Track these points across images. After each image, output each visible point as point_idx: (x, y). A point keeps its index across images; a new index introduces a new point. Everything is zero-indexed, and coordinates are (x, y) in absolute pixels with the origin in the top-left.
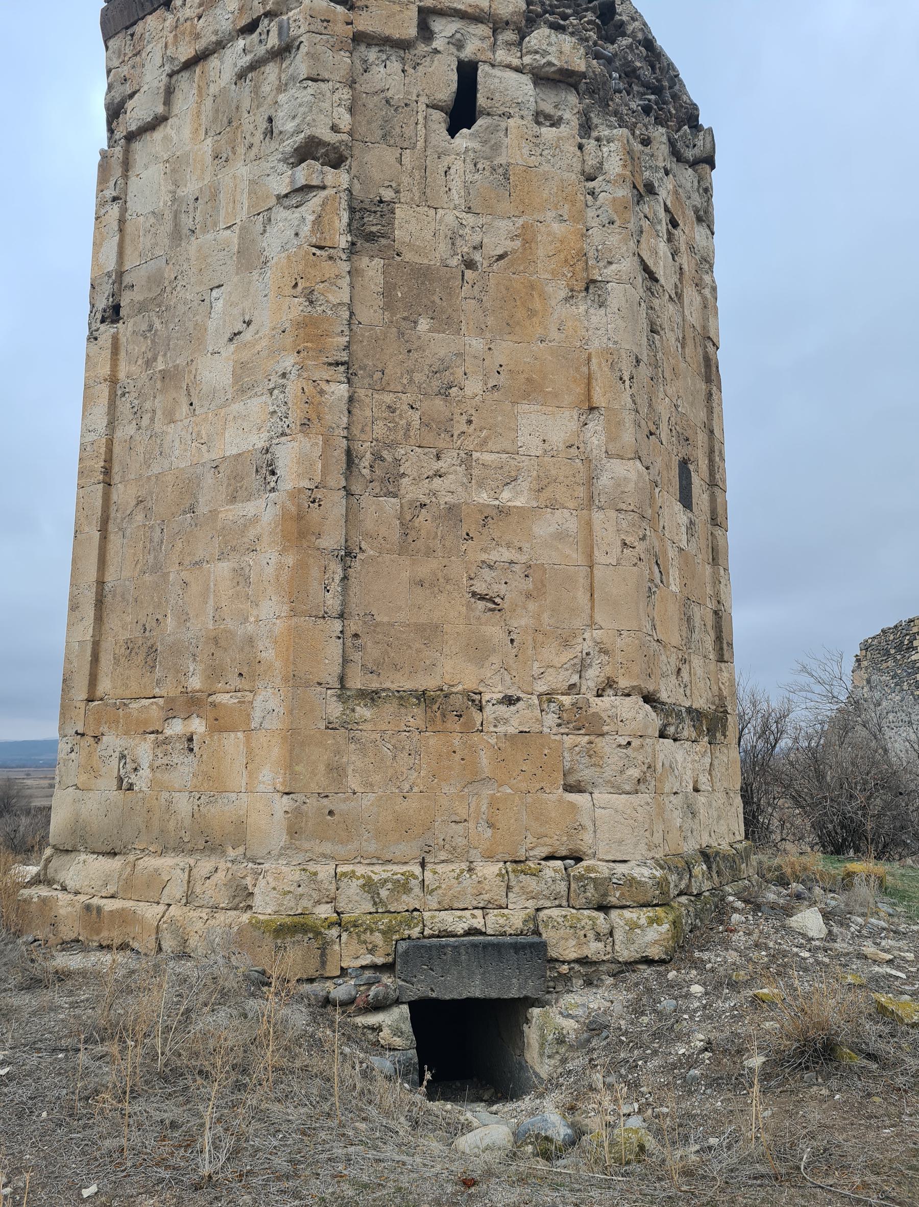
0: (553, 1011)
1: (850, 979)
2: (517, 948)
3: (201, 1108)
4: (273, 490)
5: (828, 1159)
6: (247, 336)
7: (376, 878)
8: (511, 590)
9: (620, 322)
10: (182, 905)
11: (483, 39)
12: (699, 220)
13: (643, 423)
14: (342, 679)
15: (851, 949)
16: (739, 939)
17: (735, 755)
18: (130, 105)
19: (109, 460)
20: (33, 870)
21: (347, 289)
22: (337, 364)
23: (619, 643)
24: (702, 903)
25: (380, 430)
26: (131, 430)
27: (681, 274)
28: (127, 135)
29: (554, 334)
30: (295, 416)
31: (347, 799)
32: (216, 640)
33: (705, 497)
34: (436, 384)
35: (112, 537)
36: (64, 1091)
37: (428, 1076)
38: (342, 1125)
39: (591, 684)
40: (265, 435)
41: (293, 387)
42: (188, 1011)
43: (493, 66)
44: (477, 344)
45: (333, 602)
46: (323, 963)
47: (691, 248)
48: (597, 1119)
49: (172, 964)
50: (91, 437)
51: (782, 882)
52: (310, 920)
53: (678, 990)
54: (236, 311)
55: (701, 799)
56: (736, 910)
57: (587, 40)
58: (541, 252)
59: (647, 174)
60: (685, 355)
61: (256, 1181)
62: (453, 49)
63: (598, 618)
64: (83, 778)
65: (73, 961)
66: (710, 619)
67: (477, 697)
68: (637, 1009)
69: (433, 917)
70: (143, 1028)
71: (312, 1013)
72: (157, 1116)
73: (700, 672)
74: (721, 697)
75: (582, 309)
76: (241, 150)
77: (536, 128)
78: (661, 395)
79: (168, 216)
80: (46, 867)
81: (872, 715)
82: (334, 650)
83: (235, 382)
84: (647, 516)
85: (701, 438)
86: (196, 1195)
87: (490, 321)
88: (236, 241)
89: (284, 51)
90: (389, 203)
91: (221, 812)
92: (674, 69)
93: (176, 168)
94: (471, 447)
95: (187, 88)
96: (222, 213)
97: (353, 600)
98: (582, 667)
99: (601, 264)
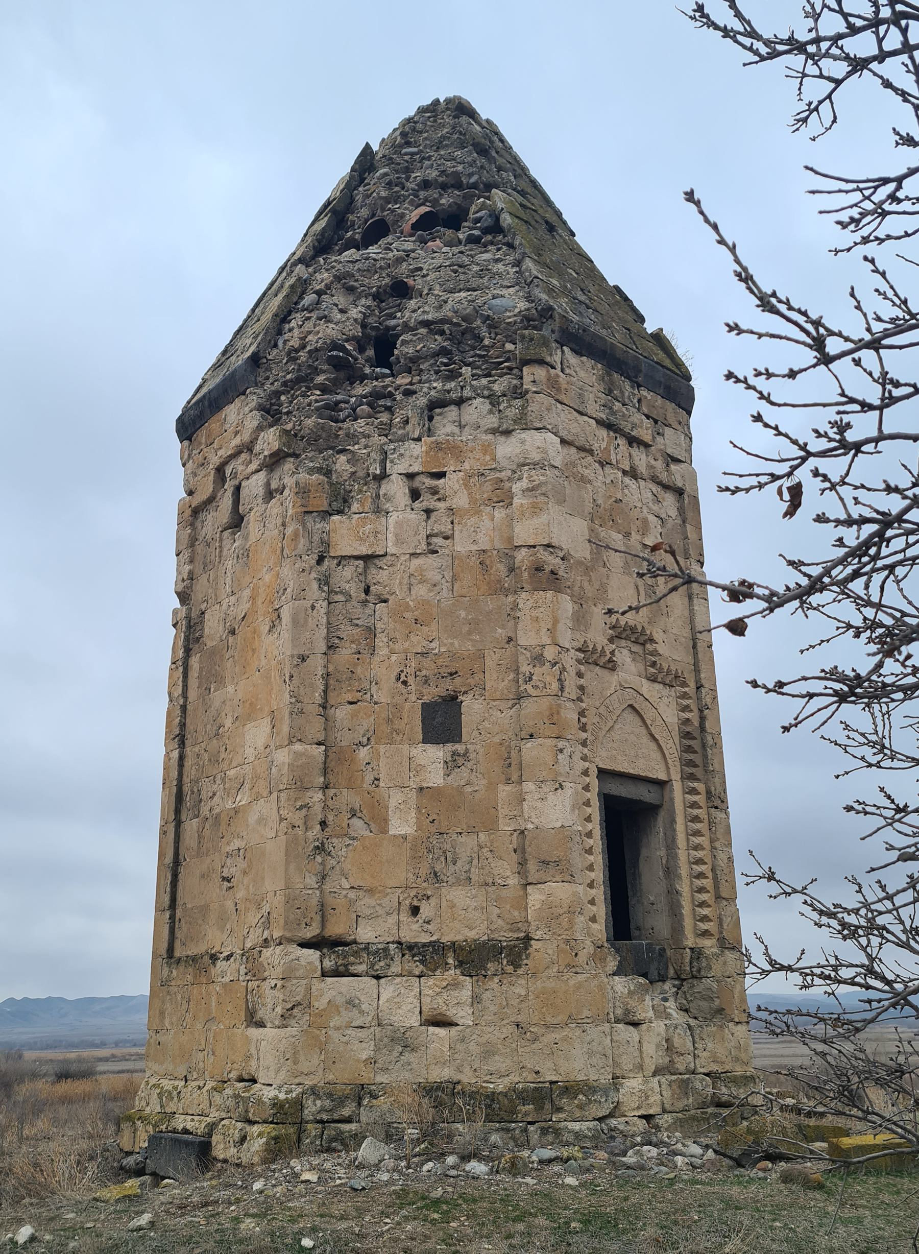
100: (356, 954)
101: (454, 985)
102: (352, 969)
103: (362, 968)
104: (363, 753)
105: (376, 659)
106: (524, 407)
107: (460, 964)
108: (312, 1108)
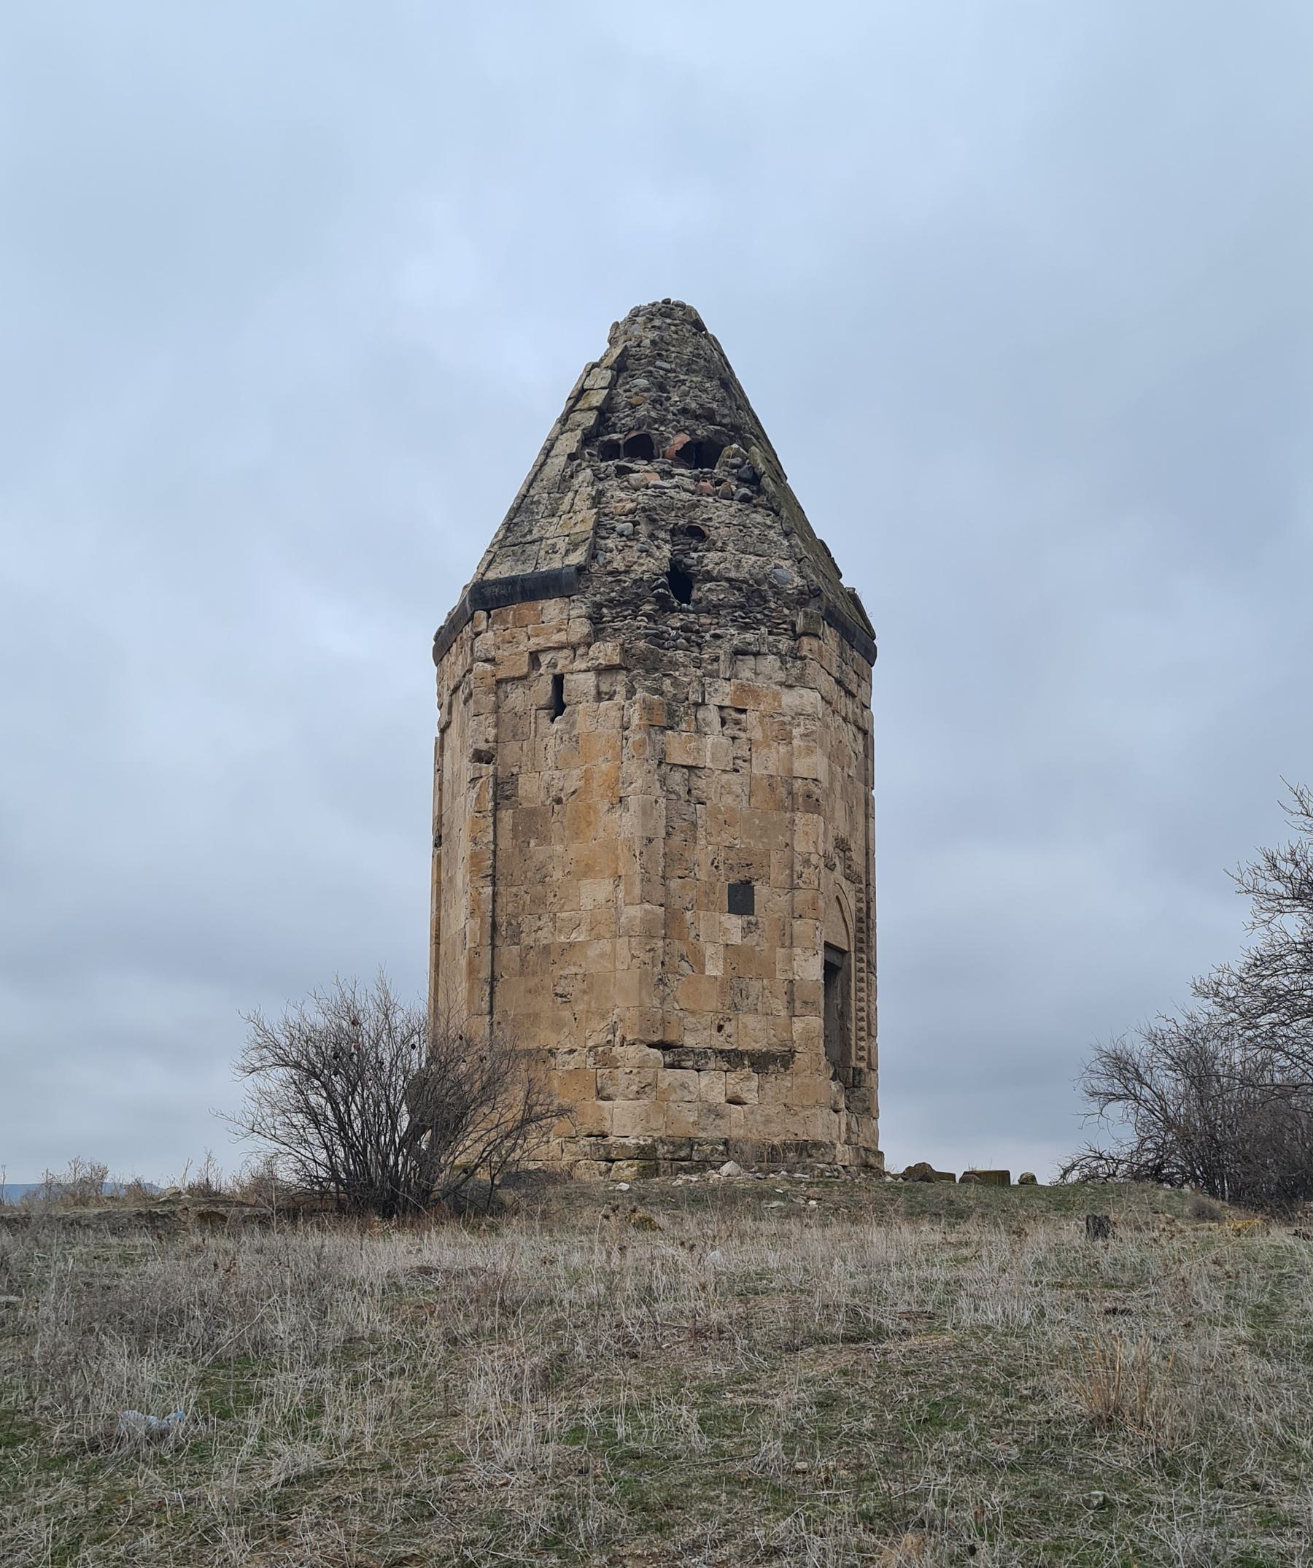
8: (574, 989)
23: (628, 1015)
25: (510, 908)
29: (602, 834)
44: (559, 848)
58: (595, 785)
87: (567, 833)
100: (686, 1054)
101: (748, 1078)
102: (683, 1064)
103: (690, 1063)
104: (688, 914)
105: (698, 847)
106: (803, 669)
107: (752, 1065)
108: (662, 1150)
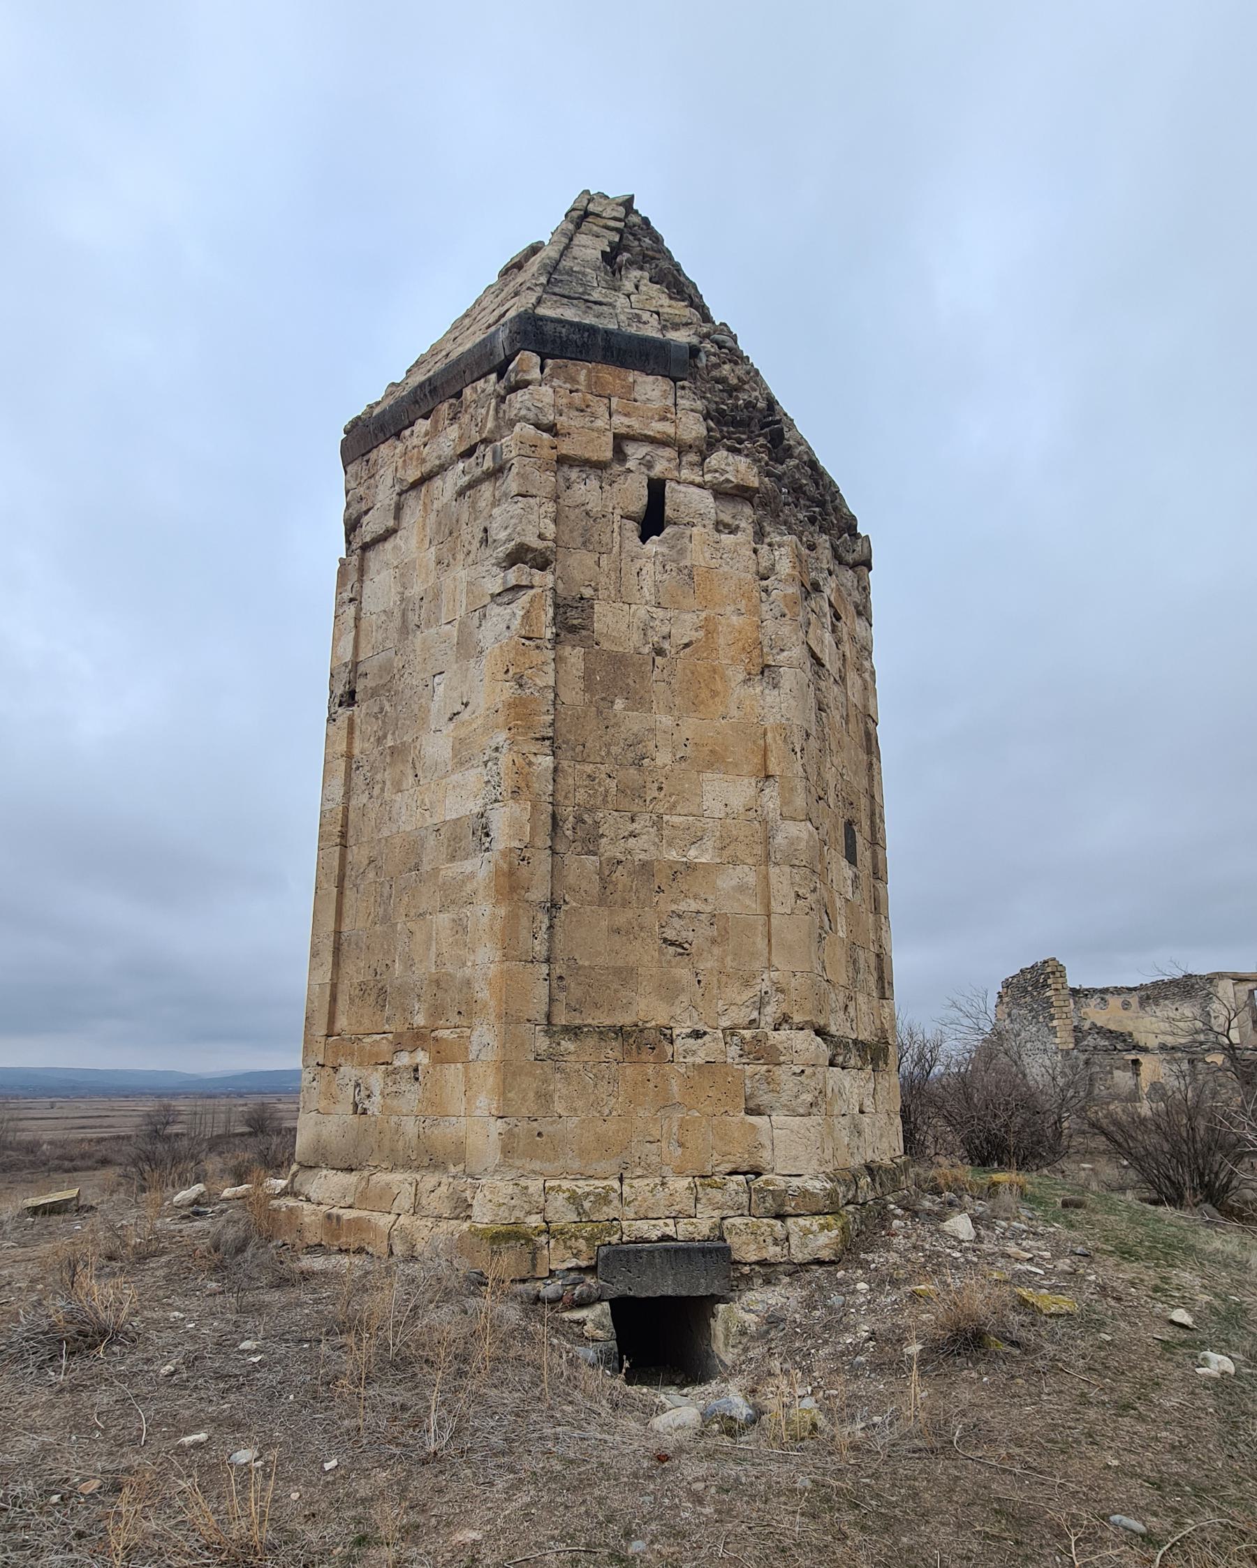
0: (736, 1306)
1: (996, 1276)
2: (704, 1252)
3: (428, 1393)
4: (487, 850)
5: (978, 1434)
6: (465, 716)
7: (579, 1191)
8: (698, 936)
9: (792, 701)
10: (412, 1215)
11: (669, 460)
12: (859, 614)
13: (813, 789)
14: (549, 1016)
15: (996, 1249)
16: (899, 1241)
17: (895, 1080)
18: (365, 520)
19: (345, 825)
20: (282, 1183)
21: (552, 674)
22: (544, 739)
23: (794, 983)
24: (867, 1210)
25: (581, 796)
26: (364, 799)
27: (844, 660)
28: (362, 543)
30: (507, 784)
31: (554, 1122)
32: (438, 982)
33: (868, 853)
34: (630, 755)
35: (348, 892)
36: (309, 1377)
37: (627, 1365)
38: (551, 1408)
39: (769, 1020)
40: (480, 802)
41: (505, 759)
42: (416, 1307)
43: (679, 483)
44: (666, 721)
45: (540, 948)
46: (534, 1266)
47: (853, 638)
48: (775, 1401)
49: (401, 1266)
50: (330, 805)
51: (937, 1191)
52: (522, 1228)
53: (845, 1286)
54: (455, 694)
55: (866, 1119)
56: (896, 1217)
57: (759, 461)
58: (722, 641)
59: (813, 574)
60: (846, 732)
61: (477, 1457)
62: (644, 469)
63: (775, 961)
64: (323, 1103)
65: (317, 1263)
66: (873, 961)
67: (668, 1032)
68: (809, 1304)
69: (630, 1226)
70: (375, 1323)
71: (524, 1310)
72: (390, 1399)
73: (864, 1008)
74: (883, 1031)
75: (758, 690)
76: (460, 556)
77: (717, 535)
78: (828, 765)
79: (397, 614)
80: (292, 1181)
81: (1012, 1044)
82: (542, 990)
83: (455, 756)
84: (817, 870)
85: (864, 802)
86: (424, 1469)
87: (678, 700)
88: (455, 634)
89: (497, 472)
90: (588, 600)
91: (445, 1132)
92: (835, 486)
93: (404, 573)
94: (662, 811)
95: (414, 505)
96: (444, 610)
97: (559, 946)
98: (761, 1005)
99: (774, 651)
